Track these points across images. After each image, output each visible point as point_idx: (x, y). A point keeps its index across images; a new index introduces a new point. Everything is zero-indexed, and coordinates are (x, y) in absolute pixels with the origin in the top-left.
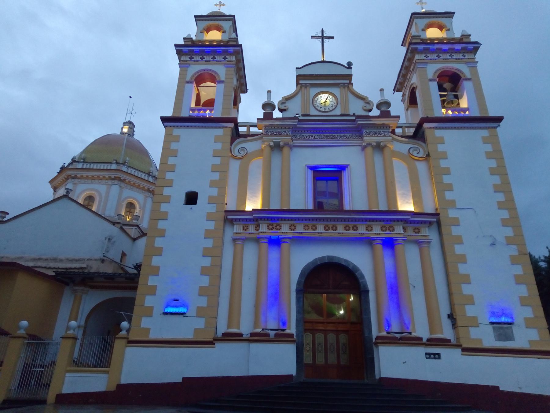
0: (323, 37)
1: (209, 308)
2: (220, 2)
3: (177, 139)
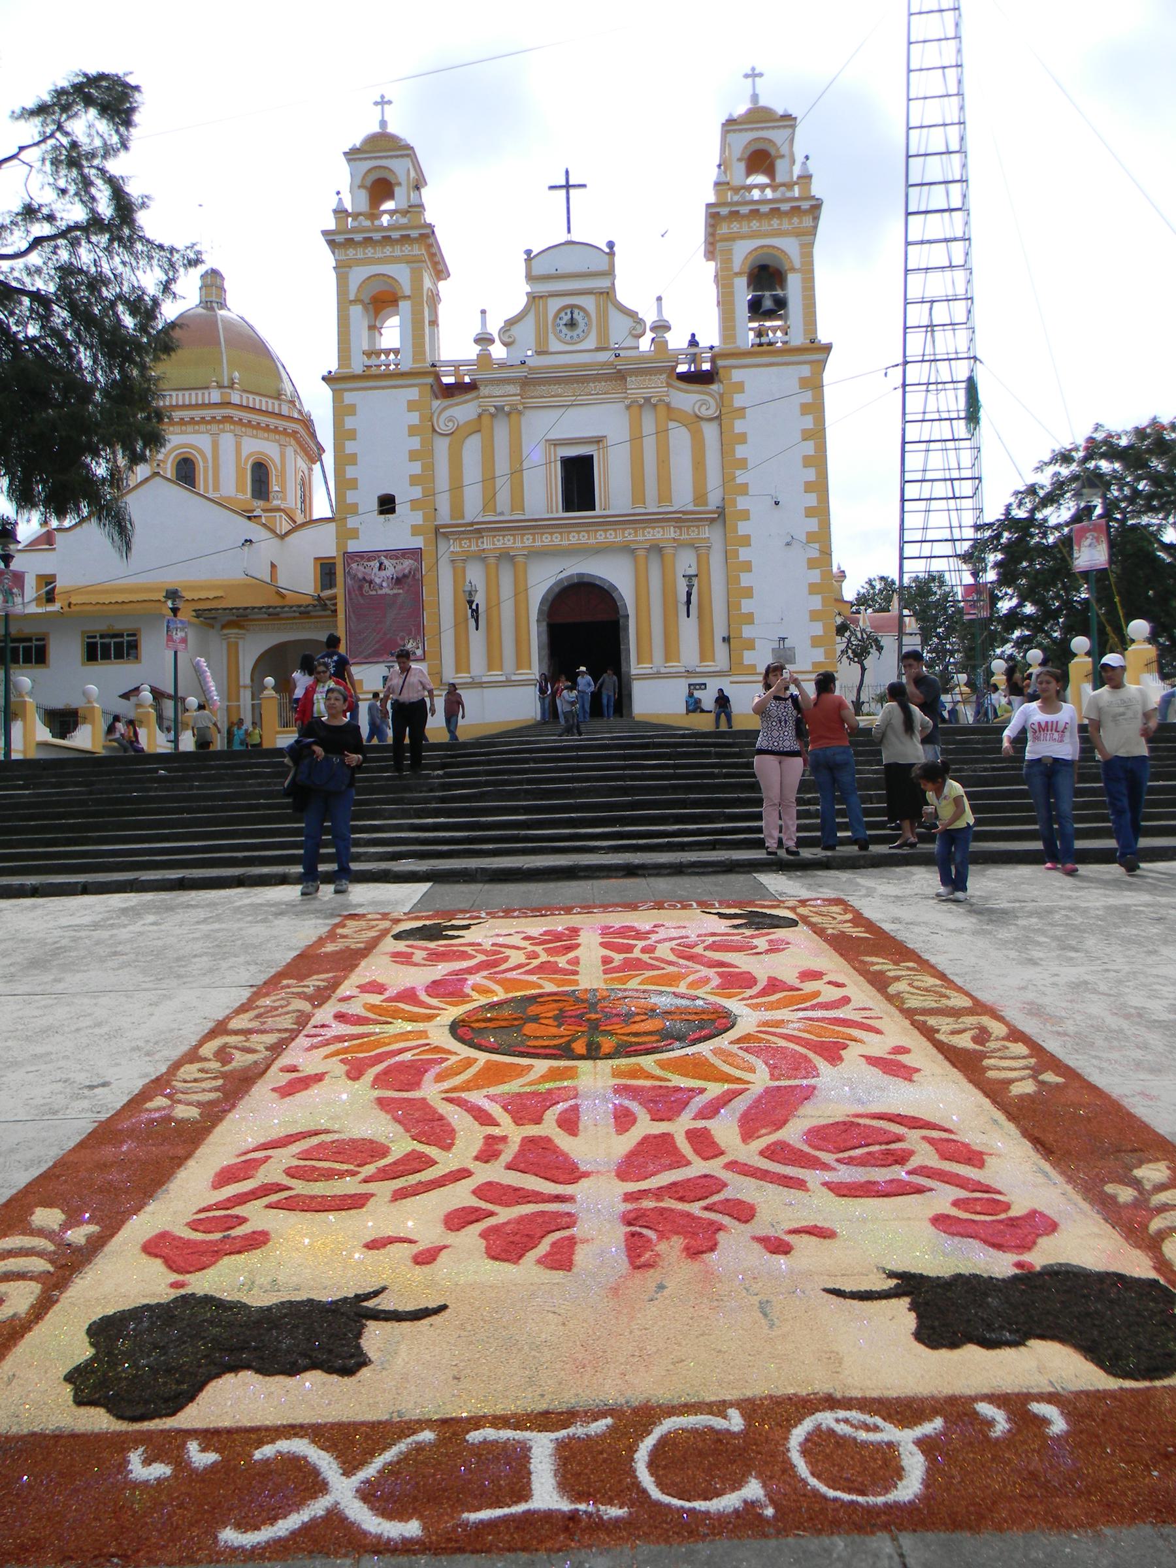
0: (567, 186)
3: (351, 410)
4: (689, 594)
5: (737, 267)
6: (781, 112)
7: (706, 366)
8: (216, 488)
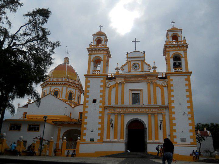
0: (136, 41)
1: (209, 142)
2: (101, 26)
3: (89, 82)
4: (161, 125)
5: (171, 57)
6: (179, 29)
7: (164, 76)
8: (61, 97)
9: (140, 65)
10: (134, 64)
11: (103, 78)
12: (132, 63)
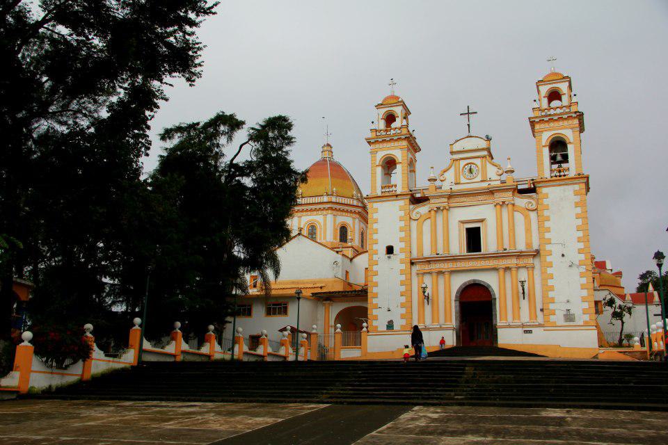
4: (523, 290)
9: (480, 166)
10: (466, 165)
11: (403, 201)
12: (463, 163)
